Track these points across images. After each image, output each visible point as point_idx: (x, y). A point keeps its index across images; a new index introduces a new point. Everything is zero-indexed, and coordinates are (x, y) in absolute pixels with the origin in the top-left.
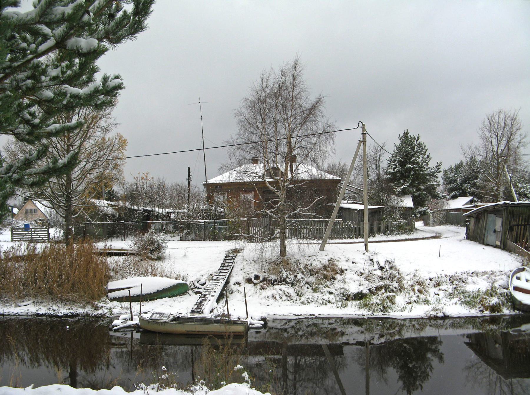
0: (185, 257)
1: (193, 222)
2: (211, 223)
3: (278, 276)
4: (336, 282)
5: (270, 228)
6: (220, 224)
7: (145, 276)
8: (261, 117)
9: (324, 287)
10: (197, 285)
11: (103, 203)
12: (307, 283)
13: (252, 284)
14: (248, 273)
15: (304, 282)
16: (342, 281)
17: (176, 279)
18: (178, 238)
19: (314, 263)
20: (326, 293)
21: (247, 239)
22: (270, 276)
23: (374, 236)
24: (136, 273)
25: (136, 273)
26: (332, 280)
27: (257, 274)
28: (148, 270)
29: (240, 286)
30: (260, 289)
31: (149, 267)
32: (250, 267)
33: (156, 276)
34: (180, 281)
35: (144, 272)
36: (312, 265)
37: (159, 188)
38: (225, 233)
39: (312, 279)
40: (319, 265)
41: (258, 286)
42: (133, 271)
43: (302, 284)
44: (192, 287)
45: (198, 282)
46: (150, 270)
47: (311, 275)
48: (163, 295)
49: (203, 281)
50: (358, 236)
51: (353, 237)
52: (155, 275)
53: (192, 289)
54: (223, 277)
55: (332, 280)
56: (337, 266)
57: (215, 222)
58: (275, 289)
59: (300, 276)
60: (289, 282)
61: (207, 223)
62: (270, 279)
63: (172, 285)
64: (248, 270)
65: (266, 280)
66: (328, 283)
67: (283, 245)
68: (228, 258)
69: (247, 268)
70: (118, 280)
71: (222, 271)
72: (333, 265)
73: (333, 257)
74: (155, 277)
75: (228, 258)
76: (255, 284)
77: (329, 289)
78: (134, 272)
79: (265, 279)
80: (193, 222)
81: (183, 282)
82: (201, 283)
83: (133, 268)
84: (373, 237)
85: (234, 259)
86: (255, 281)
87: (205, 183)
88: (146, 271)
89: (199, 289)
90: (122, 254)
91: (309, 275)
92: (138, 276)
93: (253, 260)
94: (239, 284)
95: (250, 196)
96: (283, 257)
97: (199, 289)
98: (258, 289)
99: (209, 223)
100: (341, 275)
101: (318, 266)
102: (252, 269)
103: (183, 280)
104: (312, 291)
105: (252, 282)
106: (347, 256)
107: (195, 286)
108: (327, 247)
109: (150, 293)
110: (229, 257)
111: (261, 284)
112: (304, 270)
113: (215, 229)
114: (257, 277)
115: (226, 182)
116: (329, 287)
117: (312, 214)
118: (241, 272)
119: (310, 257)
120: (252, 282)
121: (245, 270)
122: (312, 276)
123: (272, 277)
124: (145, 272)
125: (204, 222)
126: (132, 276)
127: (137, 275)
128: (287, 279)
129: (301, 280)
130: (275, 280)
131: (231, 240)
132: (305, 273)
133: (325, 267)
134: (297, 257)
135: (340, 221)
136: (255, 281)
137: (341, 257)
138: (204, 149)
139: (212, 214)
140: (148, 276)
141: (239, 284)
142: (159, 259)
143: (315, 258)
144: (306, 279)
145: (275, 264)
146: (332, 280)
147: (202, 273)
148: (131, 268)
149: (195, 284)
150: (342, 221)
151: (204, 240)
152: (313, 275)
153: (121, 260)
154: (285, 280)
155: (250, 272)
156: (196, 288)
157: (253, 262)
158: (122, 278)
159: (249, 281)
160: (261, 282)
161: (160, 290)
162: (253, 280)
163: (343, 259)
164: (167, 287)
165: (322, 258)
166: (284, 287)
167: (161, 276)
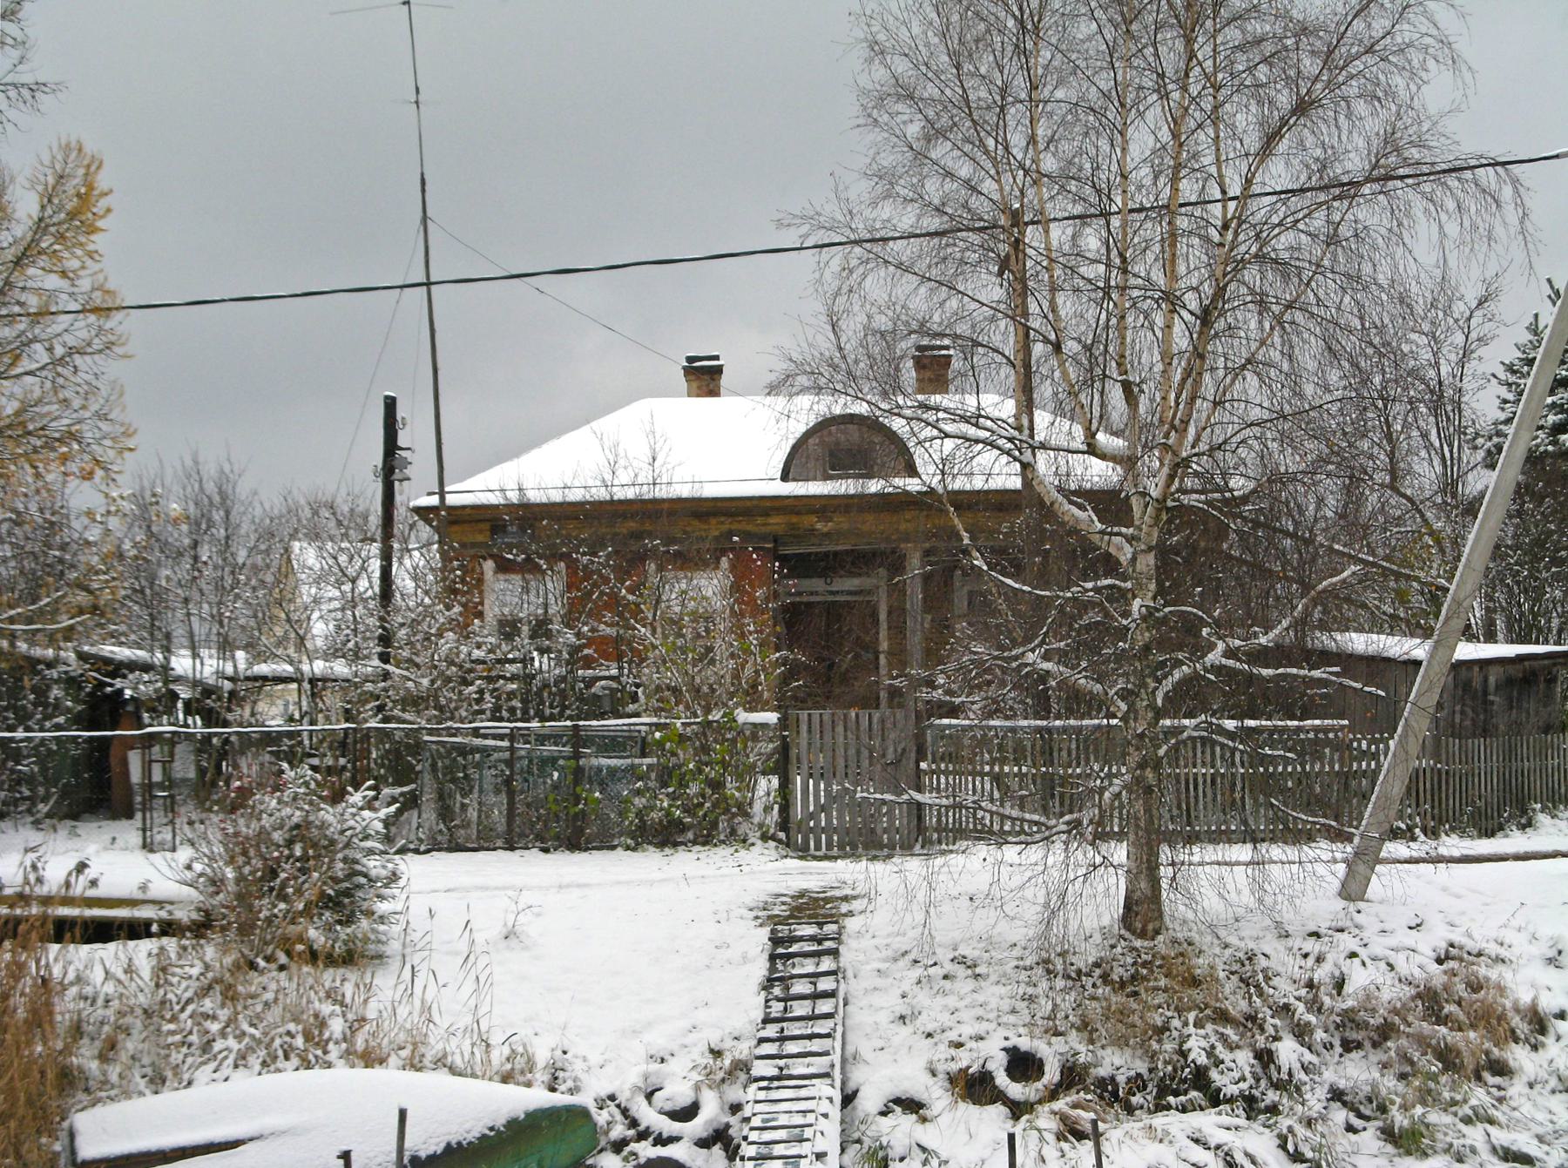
0: (513, 942)
2: (555, 738)
3: (1153, 1056)
4: (1516, 1089)
6: (612, 744)
7: (309, 1067)
9: (1467, 1121)
10: (649, 1117)
12: (1337, 1095)
13: (998, 1111)
14: (952, 1036)
15: (1322, 1093)
16: (1553, 1082)
17: (506, 1078)
18: (135, 838)
19: (1359, 978)
20: (1485, 1154)
21: (773, 838)
22: (1100, 1053)
23: (1527, 825)
24: (250, 1049)
25: (250, 1049)
26: (1492, 1080)
27: (1024, 1044)
28: (323, 1024)
29: (924, 1120)
30: (1060, 1137)
31: (326, 1008)
32: (952, 1001)
33: (382, 1061)
34: (538, 1097)
35: (299, 1042)
36: (1349, 988)
37: (199, 525)
38: (639, 802)
39: (1357, 1072)
40: (1391, 993)
41: (1045, 1120)
42: (223, 1035)
43: (1315, 1100)
44: (619, 1131)
45: (649, 1096)
46: (337, 1026)
47: (1348, 1046)
49: (678, 1091)
50: (1441, 822)
51: (1410, 829)
52: (371, 1059)
53: (618, 1146)
54: (819, 1064)
55: (1486, 1075)
56: (1501, 989)
57: (578, 739)
58: (1163, 1138)
59: (1288, 1052)
60: (1232, 1090)
62: (1103, 1072)
63: (500, 1122)
64: (946, 1019)
65: (1082, 1080)
66: (1479, 1096)
67: (1146, 869)
68: (795, 948)
69: (934, 1011)
70: (127, 1095)
71: (794, 1029)
72: (1475, 986)
73: (1457, 938)
74: (377, 1072)
75: (795, 948)
76: (1018, 1109)
77: (1501, 1137)
78: (231, 1042)
79: (1072, 1076)
81: (560, 1099)
82: (668, 1107)
83: (224, 1014)
84: (1523, 827)
85: (834, 953)
86: (1016, 1090)
87: (434, 500)
88: (315, 1033)
89: (661, 1141)
90: (137, 930)
91: (1338, 1050)
92: (264, 1064)
93: (960, 961)
94: (912, 1105)
95: (711, 586)
96: (1142, 935)
97: (661, 1141)
98: (1050, 1137)
99: (542, 739)
100: (1535, 1048)
101: (1386, 995)
102: (964, 1015)
103: (553, 1090)
104: (1390, 1148)
105: (998, 1096)
106: (1546, 931)
107: (634, 1123)
108: (1382, 882)
110: (794, 940)
111: (1060, 1105)
112: (1312, 1019)
113: (576, 782)
114: (1023, 1065)
115: (630, 494)
116: (1491, 1121)
117: (1316, 674)
118: (905, 1031)
119: (1316, 935)
120: (998, 1096)
121: (927, 1022)
122: (1354, 1055)
123: (1118, 1061)
124: (308, 1037)
125: (512, 736)
126: (226, 1070)
127: (255, 1061)
128: (1214, 1074)
129: (1303, 1076)
130: (1138, 1083)
131: (675, 845)
132: (1320, 1035)
133: (1431, 1001)
134: (1242, 938)
136: (1016, 1090)
137: (1509, 936)
138: (428, 284)
139: (537, 682)
140: (329, 1065)
141: (912, 1105)
142: (349, 958)
143: (1348, 942)
144: (1329, 1076)
145: (1105, 978)
146: (1486, 1075)
147: (659, 1040)
148: (214, 1018)
149: (634, 1112)
151: (511, 847)
152: (1359, 1046)
153: (145, 967)
154: (1200, 1079)
155: (967, 1030)
156: (642, 1136)
157: (961, 971)
158: (157, 1082)
160: (1053, 1094)
161: (432, 1158)
162: (1002, 1080)
163: (1520, 946)
164: (473, 1136)
165: (1392, 941)
166: (1209, 1122)
167: (414, 1064)
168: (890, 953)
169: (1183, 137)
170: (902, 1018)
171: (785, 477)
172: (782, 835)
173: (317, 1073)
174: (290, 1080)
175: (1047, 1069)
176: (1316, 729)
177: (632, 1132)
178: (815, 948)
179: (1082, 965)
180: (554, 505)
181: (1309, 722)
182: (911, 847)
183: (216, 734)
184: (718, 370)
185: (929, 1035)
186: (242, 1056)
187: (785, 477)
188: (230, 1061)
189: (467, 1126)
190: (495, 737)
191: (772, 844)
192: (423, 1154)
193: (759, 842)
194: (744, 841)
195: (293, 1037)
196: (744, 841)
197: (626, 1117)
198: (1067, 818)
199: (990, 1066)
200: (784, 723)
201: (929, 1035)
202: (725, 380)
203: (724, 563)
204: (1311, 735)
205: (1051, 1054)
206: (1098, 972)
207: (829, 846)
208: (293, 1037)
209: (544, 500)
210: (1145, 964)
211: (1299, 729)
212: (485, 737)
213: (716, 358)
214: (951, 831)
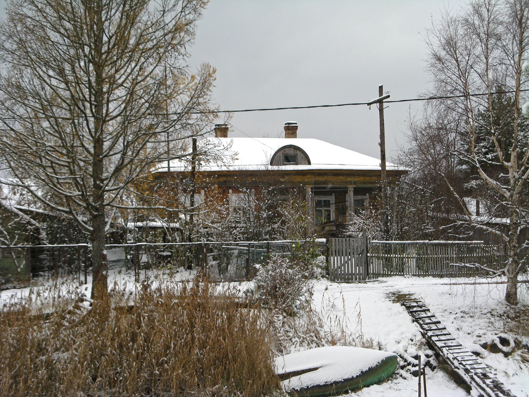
1: (227, 245)
2: (261, 247)
5: (367, 256)
7: (319, 346)
8: (29, 17)
11: (464, 167)
24: (303, 341)
27: (503, 335)
33: (336, 344)
48: (369, 380)
57: (268, 246)
61: (253, 247)
63: (380, 361)
78: (297, 339)
80: (227, 245)
86: (505, 349)
109: (351, 377)
125: (249, 246)
135: (480, 244)
145: (508, 317)
150: (484, 244)
159: (493, 348)
161: (366, 371)
162: (500, 346)
164: (374, 365)
167: (345, 344)
168: (441, 310)
169: (161, 55)
170: (458, 329)
171: (271, 164)
172: (327, 276)
173: (321, 348)
174: (315, 351)
175: (511, 342)
176: (475, 244)
177: (406, 363)
178: (420, 309)
179: (501, 313)
180: (236, 171)
181: (474, 242)
182: (365, 279)
183: (143, 245)
184: (296, 127)
185: (469, 334)
186: (301, 343)
187: (271, 164)
188: (298, 344)
189: (373, 362)
190: (243, 246)
191: (325, 278)
192: (364, 371)
193: (321, 278)
194: (316, 278)
195: (312, 337)
196: (316, 278)
197: (403, 359)
198: (500, 270)
199: (495, 342)
200: (327, 241)
201: (469, 334)
202: (298, 131)
203: (203, 192)
204: (473, 245)
205: (510, 337)
206: (505, 315)
207: (360, 279)
208: (312, 337)
209: (244, 169)
210: (518, 312)
211: (470, 244)
212: (240, 246)
213: (296, 124)
214: (358, 274)
